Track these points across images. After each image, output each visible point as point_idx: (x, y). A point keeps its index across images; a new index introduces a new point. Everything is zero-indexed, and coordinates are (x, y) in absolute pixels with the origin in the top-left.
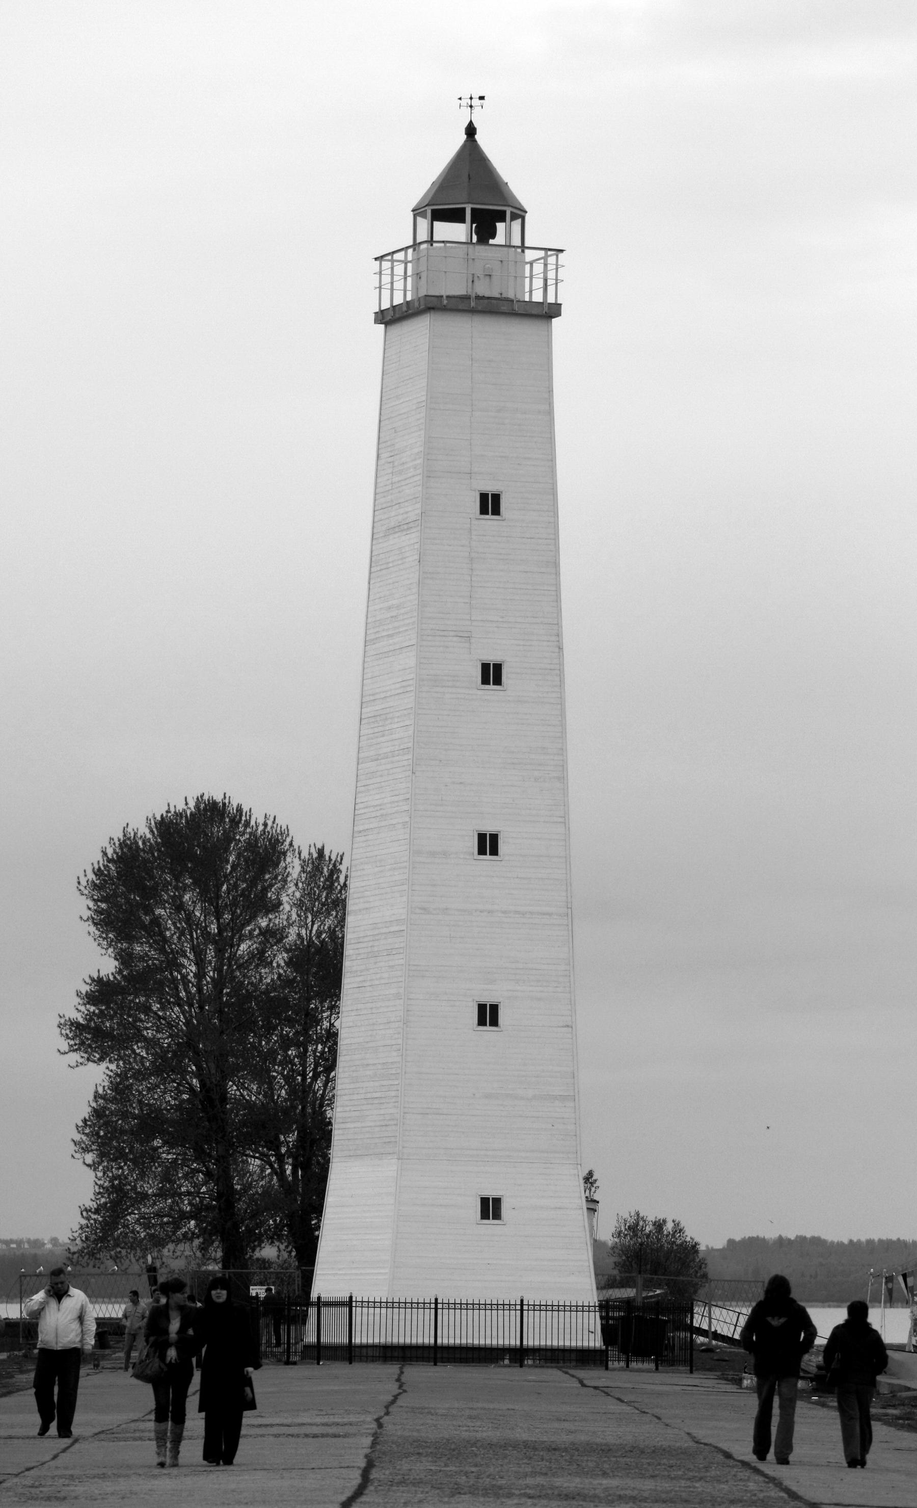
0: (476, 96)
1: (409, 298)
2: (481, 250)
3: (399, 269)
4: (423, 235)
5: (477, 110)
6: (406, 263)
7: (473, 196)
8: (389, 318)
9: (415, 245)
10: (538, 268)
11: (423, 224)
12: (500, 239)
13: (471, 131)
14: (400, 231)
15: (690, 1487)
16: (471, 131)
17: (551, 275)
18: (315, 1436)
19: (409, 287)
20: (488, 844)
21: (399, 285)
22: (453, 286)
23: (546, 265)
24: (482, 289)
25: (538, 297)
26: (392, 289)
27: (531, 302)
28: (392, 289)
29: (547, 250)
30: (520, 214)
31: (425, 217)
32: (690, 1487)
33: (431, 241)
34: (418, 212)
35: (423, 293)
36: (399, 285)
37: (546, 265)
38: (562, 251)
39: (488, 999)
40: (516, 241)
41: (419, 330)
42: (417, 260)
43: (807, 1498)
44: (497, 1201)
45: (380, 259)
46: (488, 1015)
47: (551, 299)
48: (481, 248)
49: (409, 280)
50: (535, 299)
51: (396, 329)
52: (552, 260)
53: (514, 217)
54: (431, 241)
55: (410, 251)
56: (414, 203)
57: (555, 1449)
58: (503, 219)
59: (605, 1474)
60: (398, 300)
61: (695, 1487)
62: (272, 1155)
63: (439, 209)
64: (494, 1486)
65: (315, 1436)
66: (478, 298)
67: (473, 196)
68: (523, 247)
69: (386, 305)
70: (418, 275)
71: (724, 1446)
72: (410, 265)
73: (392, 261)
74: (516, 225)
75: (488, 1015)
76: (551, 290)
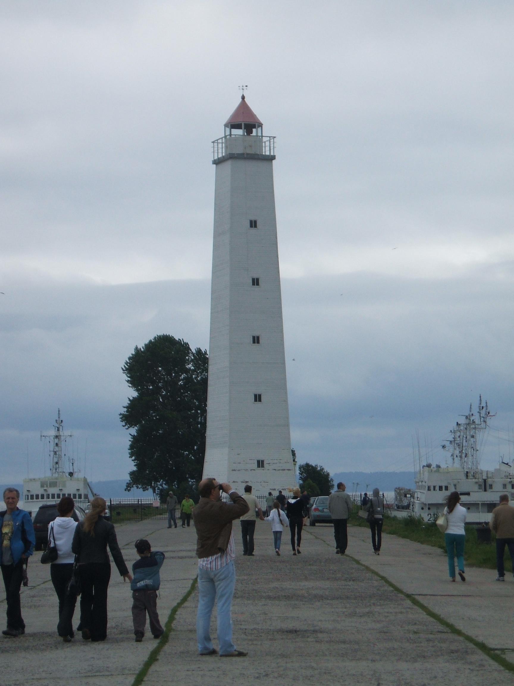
0: (244, 86)
1: (224, 155)
2: (248, 138)
3: (220, 145)
4: (228, 133)
5: (245, 90)
6: (222, 143)
7: (244, 121)
8: (217, 162)
9: (225, 137)
10: (267, 144)
11: (228, 130)
12: (254, 133)
13: (243, 98)
14: (220, 132)
15: (346, 585)
16: (243, 98)
17: (272, 145)
18: (182, 558)
19: (224, 151)
20: (256, 340)
21: (220, 151)
22: (239, 150)
23: (270, 142)
24: (249, 151)
25: (268, 153)
26: (218, 153)
27: (265, 155)
28: (218, 153)
29: (270, 137)
30: (260, 125)
31: (228, 127)
32: (346, 585)
33: (231, 135)
34: (226, 126)
35: (228, 153)
36: (220, 151)
37: (270, 142)
38: (275, 137)
39: (258, 393)
40: (260, 134)
41: (228, 166)
42: (226, 141)
43: (404, 591)
44: (263, 461)
45: (213, 142)
46: (258, 398)
47: (272, 154)
48: (248, 137)
49: (224, 149)
50: (266, 154)
51: (220, 166)
52: (272, 140)
53: (259, 127)
54: (231, 135)
55: (224, 139)
56: (224, 123)
57: (283, 562)
58: (255, 127)
59: (306, 579)
60: (220, 156)
61: (349, 585)
62: (378, 513)
63: (233, 125)
64: (254, 590)
65: (182, 558)
66: (247, 154)
67: (244, 121)
68: (262, 136)
69: (216, 158)
70: (226, 147)
71: (356, 558)
72: (224, 144)
73: (218, 143)
74: (259, 129)
75: (258, 398)
76: (272, 151)
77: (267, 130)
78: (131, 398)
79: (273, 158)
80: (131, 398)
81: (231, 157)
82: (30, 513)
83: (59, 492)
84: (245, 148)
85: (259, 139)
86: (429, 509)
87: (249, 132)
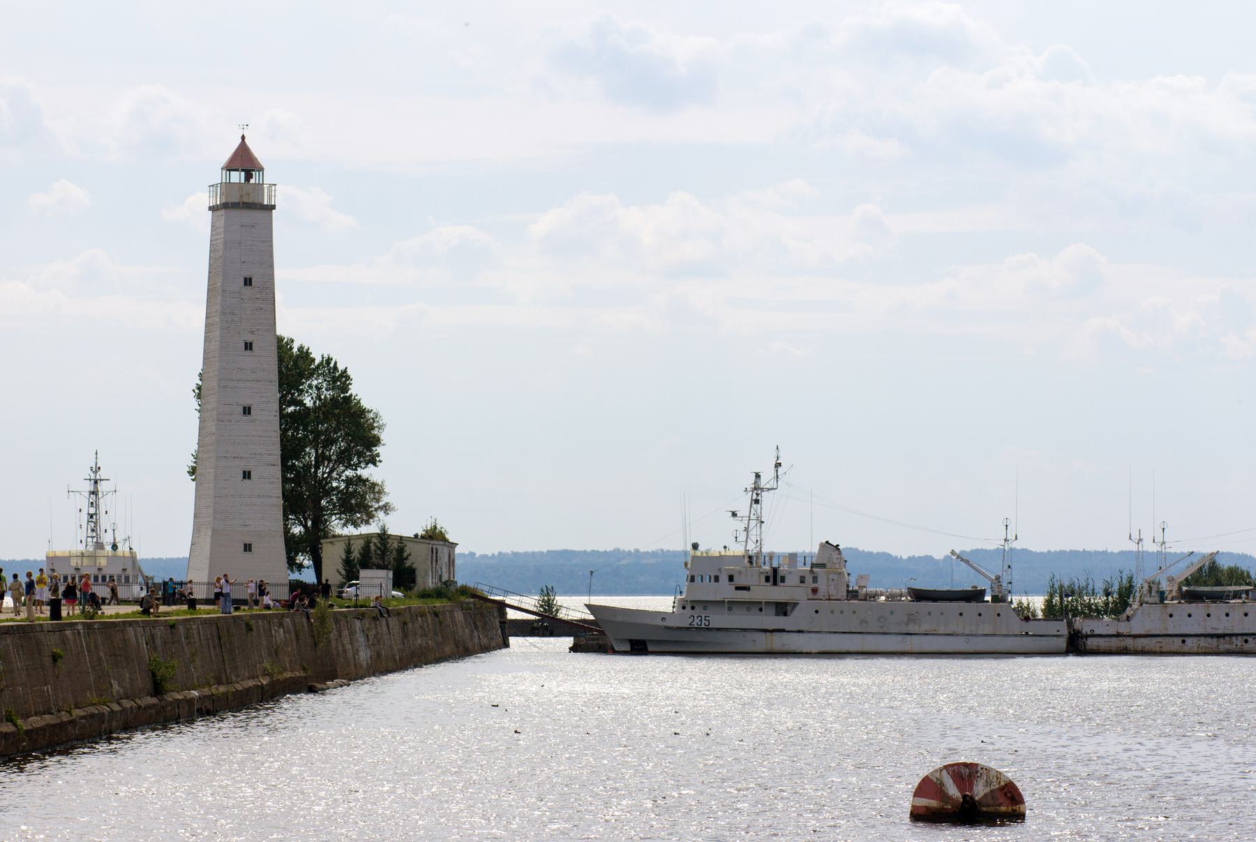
7: (243, 161)
8: (211, 208)
13: (243, 138)
16: (243, 138)
22: (235, 199)
30: (261, 169)
39: (247, 469)
63: (230, 168)
67: (243, 161)
77: (268, 178)
78: (123, 549)
79: (273, 207)
80: (123, 549)
81: (225, 206)
82: (373, 461)
83: (96, 572)
84: (244, 202)
85: (260, 186)
86: (693, 608)
87: (248, 176)
